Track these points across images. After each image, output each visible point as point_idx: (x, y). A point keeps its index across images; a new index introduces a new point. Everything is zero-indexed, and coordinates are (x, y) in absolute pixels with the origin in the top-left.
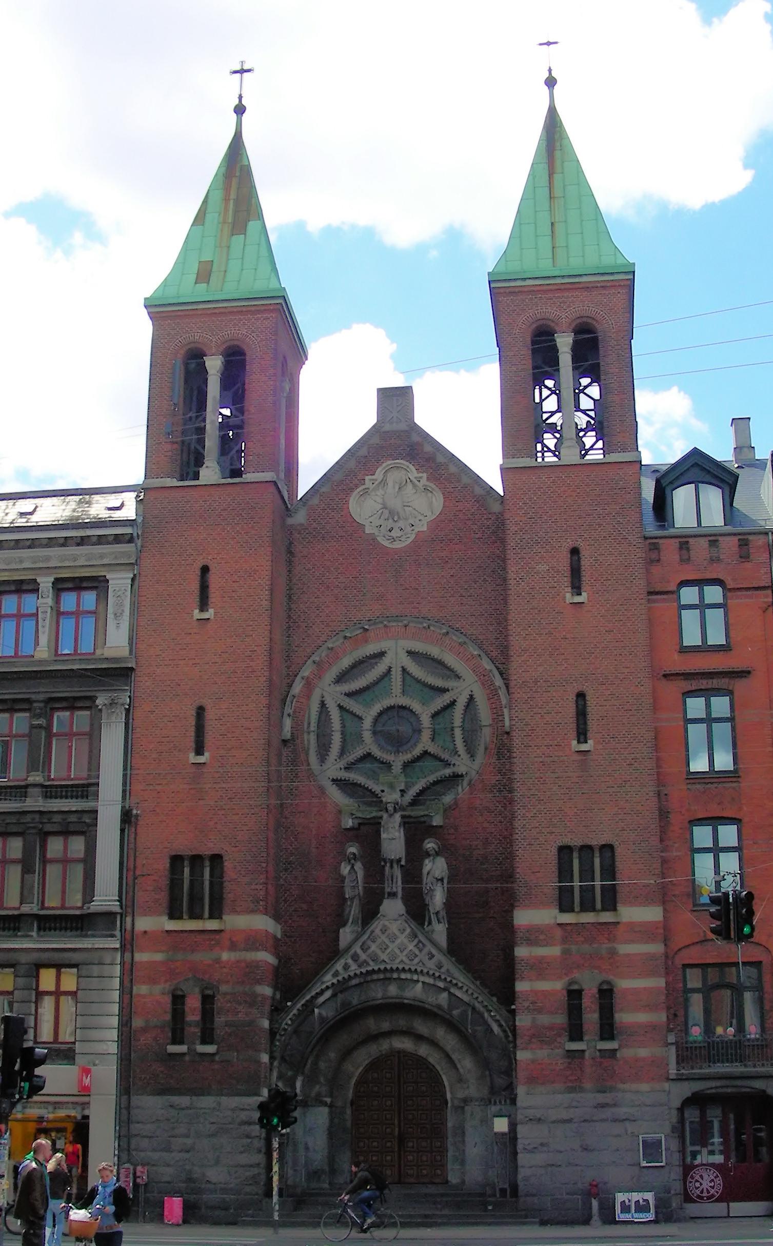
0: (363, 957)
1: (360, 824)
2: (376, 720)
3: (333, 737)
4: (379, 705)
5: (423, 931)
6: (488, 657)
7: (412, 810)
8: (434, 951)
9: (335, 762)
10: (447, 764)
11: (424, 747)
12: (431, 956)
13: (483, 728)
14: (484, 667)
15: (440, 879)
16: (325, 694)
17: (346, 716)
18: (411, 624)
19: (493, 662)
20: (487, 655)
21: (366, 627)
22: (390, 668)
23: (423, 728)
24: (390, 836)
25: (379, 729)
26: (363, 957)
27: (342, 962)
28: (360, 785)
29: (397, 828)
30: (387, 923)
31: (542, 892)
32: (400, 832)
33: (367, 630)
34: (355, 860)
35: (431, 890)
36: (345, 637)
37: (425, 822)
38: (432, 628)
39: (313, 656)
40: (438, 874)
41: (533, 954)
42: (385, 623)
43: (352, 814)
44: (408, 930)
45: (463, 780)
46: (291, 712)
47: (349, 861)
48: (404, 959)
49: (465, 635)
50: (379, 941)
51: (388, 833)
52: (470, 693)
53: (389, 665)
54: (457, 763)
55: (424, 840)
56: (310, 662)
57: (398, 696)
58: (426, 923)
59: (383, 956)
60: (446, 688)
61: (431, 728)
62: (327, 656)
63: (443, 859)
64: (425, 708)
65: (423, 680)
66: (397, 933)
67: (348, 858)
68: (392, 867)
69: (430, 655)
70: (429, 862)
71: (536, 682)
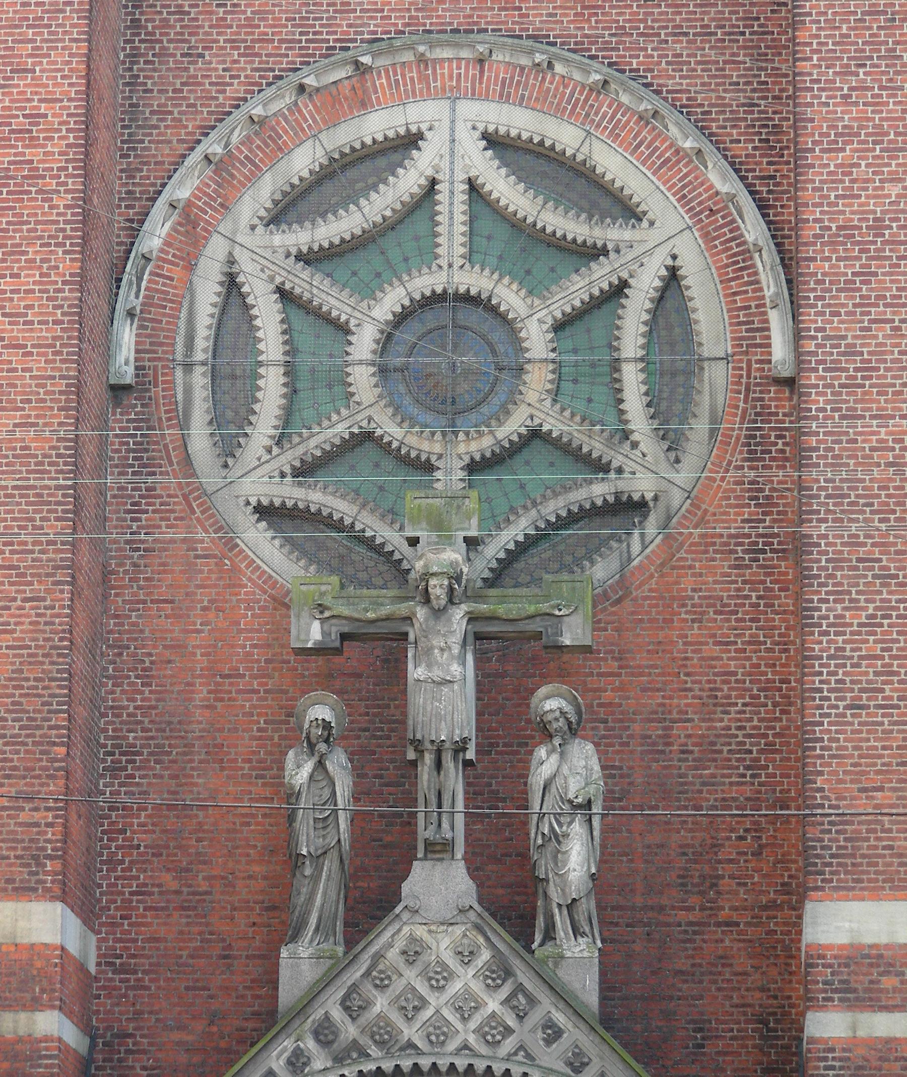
0: (350, 1031)
1: (344, 637)
2: (386, 341)
3: (261, 383)
4: (400, 292)
5: (527, 956)
6: (725, 157)
7: (502, 599)
8: (560, 1018)
9: (266, 457)
10: (601, 467)
11: (532, 417)
12: (553, 1033)
13: (706, 364)
14: (711, 186)
15: (580, 806)
16: (237, 252)
17: (298, 319)
18: (498, 56)
19: (737, 171)
20: (723, 152)
21: (366, 60)
22: (433, 182)
23: (529, 361)
24: (437, 674)
25: (399, 361)
26: (350, 1031)
27: (288, 1044)
28: (338, 526)
29: (456, 650)
30: (421, 932)
31: (891, 848)
32: (464, 664)
33: (368, 69)
34: (327, 741)
35: (558, 838)
36: (302, 88)
37: (538, 636)
38: (559, 68)
39: (206, 142)
40: (574, 788)
41: (861, 1033)
42: (421, 49)
43: (322, 608)
44: (485, 955)
45: (645, 516)
46: (137, 303)
47: (312, 746)
48: (472, 1039)
49: (658, 92)
50: (398, 986)
51: (429, 666)
52: (670, 262)
53: (429, 172)
54: (629, 466)
55: (532, 691)
56: (195, 157)
57: (455, 267)
58: (538, 938)
59: (410, 1032)
60: (600, 244)
61: (553, 361)
62: (247, 141)
63: (590, 747)
64: (537, 302)
65: (530, 220)
66: (451, 962)
67: (308, 737)
68: (439, 765)
69: (552, 147)
70: (549, 754)
71: (878, 227)
